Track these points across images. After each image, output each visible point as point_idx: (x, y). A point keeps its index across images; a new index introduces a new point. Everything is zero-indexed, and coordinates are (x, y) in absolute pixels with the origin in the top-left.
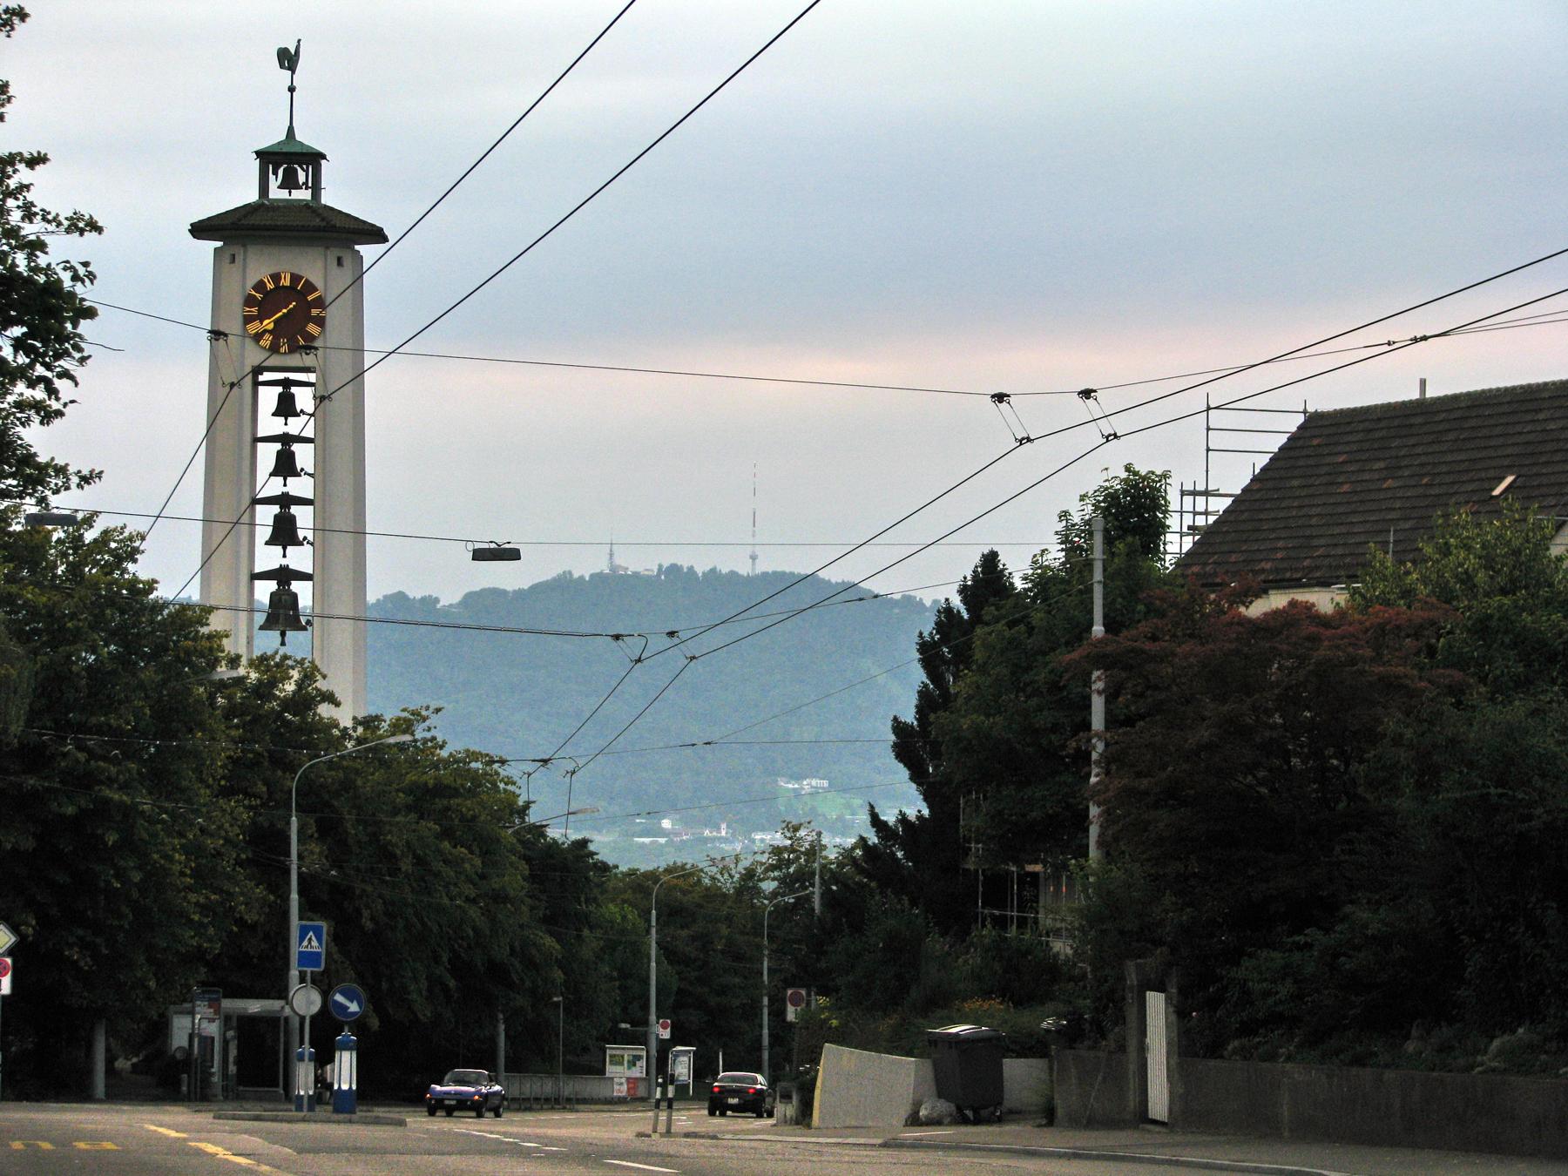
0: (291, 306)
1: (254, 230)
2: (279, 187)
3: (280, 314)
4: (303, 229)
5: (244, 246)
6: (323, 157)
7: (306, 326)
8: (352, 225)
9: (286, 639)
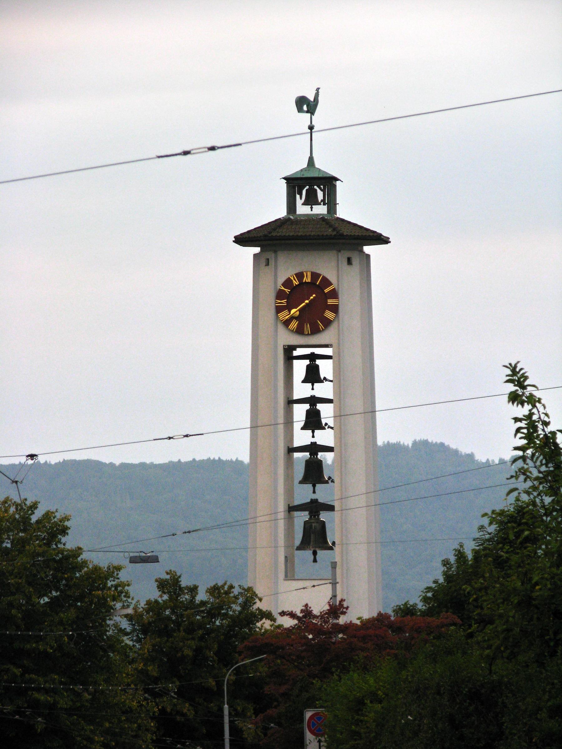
0: (312, 298)
1: (280, 240)
2: (303, 204)
3: (303, 304)
4: (318, 238)
5: (275, 252)
6: (336, 179)
7: (324, 312)
8: (357, 233)
9: (317, 557)
